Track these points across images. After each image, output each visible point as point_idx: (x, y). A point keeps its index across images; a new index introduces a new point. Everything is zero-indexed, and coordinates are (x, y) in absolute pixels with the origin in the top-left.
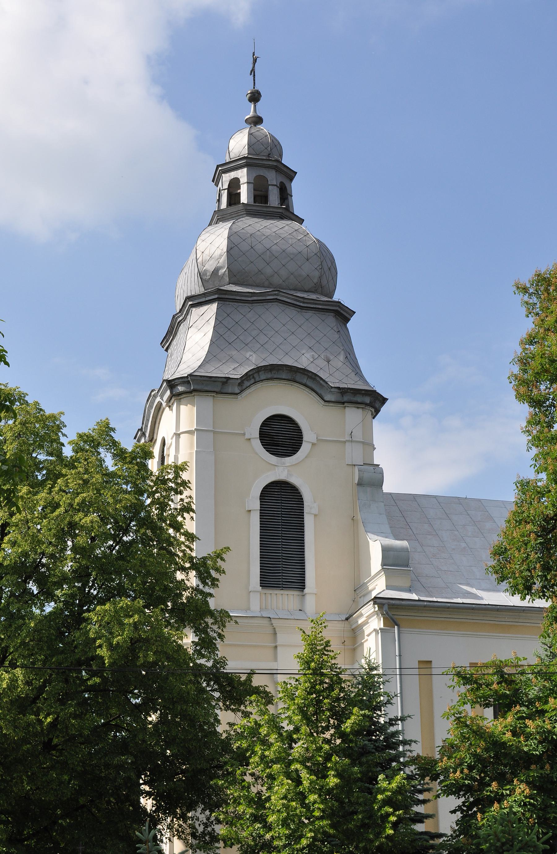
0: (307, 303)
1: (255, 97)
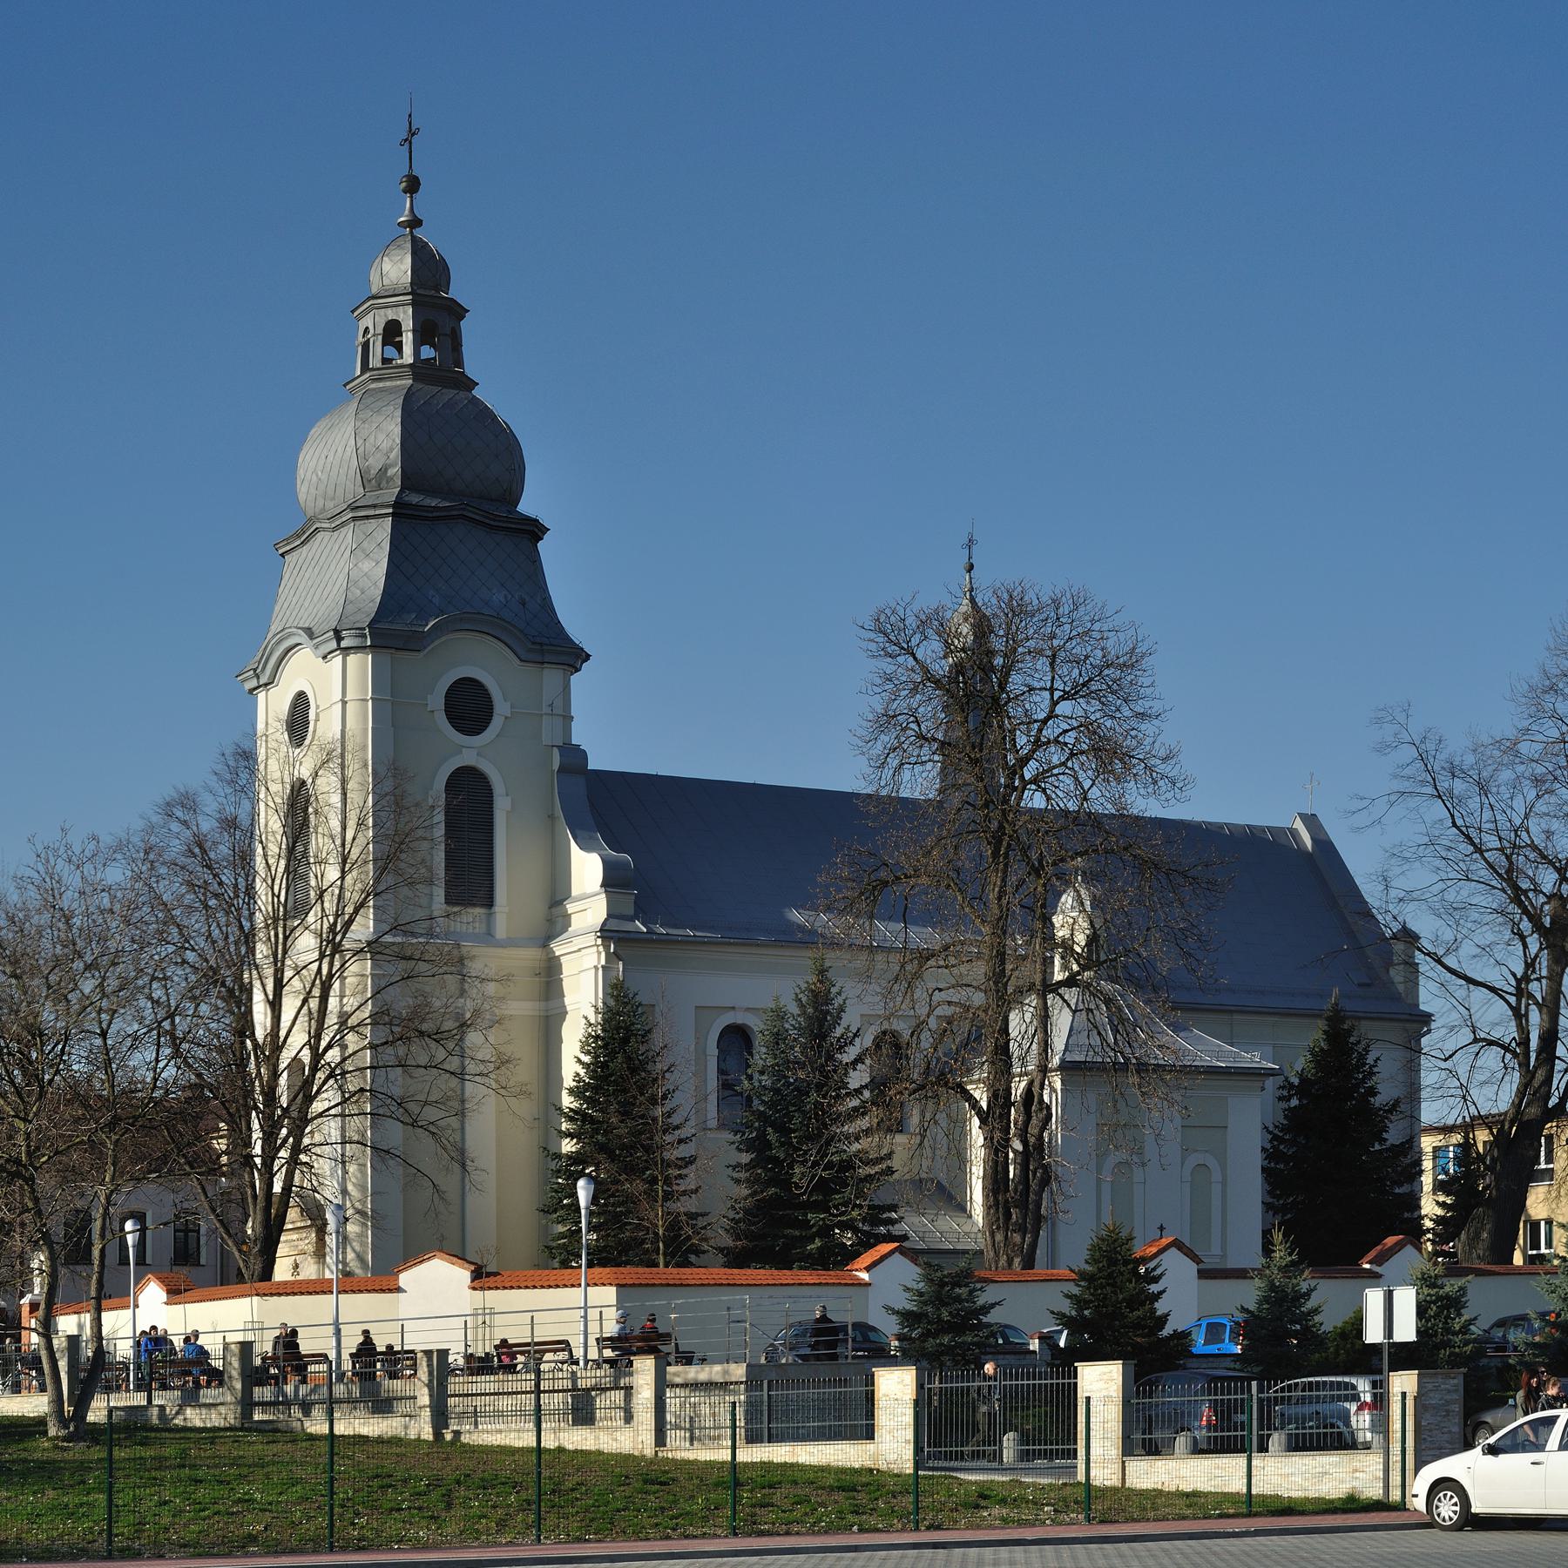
0: (500, 521)
1: (413, 185)
